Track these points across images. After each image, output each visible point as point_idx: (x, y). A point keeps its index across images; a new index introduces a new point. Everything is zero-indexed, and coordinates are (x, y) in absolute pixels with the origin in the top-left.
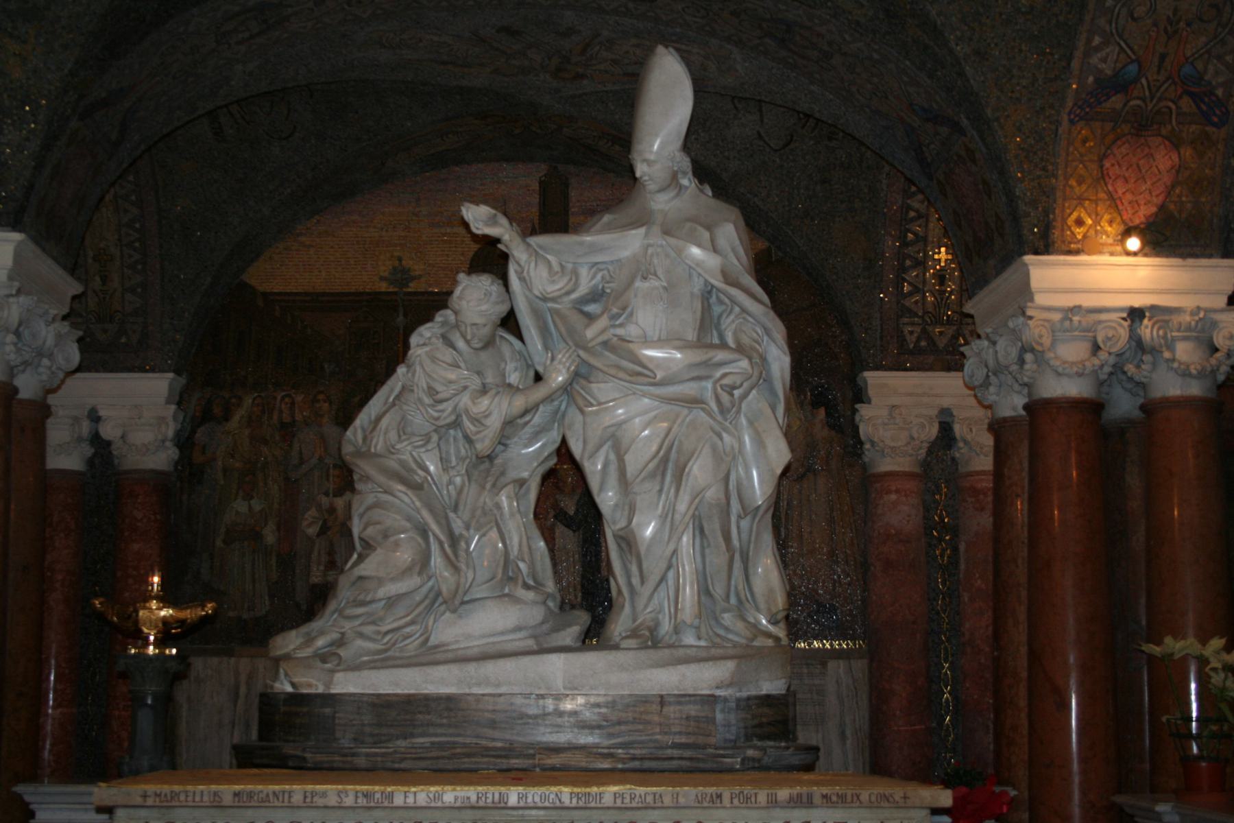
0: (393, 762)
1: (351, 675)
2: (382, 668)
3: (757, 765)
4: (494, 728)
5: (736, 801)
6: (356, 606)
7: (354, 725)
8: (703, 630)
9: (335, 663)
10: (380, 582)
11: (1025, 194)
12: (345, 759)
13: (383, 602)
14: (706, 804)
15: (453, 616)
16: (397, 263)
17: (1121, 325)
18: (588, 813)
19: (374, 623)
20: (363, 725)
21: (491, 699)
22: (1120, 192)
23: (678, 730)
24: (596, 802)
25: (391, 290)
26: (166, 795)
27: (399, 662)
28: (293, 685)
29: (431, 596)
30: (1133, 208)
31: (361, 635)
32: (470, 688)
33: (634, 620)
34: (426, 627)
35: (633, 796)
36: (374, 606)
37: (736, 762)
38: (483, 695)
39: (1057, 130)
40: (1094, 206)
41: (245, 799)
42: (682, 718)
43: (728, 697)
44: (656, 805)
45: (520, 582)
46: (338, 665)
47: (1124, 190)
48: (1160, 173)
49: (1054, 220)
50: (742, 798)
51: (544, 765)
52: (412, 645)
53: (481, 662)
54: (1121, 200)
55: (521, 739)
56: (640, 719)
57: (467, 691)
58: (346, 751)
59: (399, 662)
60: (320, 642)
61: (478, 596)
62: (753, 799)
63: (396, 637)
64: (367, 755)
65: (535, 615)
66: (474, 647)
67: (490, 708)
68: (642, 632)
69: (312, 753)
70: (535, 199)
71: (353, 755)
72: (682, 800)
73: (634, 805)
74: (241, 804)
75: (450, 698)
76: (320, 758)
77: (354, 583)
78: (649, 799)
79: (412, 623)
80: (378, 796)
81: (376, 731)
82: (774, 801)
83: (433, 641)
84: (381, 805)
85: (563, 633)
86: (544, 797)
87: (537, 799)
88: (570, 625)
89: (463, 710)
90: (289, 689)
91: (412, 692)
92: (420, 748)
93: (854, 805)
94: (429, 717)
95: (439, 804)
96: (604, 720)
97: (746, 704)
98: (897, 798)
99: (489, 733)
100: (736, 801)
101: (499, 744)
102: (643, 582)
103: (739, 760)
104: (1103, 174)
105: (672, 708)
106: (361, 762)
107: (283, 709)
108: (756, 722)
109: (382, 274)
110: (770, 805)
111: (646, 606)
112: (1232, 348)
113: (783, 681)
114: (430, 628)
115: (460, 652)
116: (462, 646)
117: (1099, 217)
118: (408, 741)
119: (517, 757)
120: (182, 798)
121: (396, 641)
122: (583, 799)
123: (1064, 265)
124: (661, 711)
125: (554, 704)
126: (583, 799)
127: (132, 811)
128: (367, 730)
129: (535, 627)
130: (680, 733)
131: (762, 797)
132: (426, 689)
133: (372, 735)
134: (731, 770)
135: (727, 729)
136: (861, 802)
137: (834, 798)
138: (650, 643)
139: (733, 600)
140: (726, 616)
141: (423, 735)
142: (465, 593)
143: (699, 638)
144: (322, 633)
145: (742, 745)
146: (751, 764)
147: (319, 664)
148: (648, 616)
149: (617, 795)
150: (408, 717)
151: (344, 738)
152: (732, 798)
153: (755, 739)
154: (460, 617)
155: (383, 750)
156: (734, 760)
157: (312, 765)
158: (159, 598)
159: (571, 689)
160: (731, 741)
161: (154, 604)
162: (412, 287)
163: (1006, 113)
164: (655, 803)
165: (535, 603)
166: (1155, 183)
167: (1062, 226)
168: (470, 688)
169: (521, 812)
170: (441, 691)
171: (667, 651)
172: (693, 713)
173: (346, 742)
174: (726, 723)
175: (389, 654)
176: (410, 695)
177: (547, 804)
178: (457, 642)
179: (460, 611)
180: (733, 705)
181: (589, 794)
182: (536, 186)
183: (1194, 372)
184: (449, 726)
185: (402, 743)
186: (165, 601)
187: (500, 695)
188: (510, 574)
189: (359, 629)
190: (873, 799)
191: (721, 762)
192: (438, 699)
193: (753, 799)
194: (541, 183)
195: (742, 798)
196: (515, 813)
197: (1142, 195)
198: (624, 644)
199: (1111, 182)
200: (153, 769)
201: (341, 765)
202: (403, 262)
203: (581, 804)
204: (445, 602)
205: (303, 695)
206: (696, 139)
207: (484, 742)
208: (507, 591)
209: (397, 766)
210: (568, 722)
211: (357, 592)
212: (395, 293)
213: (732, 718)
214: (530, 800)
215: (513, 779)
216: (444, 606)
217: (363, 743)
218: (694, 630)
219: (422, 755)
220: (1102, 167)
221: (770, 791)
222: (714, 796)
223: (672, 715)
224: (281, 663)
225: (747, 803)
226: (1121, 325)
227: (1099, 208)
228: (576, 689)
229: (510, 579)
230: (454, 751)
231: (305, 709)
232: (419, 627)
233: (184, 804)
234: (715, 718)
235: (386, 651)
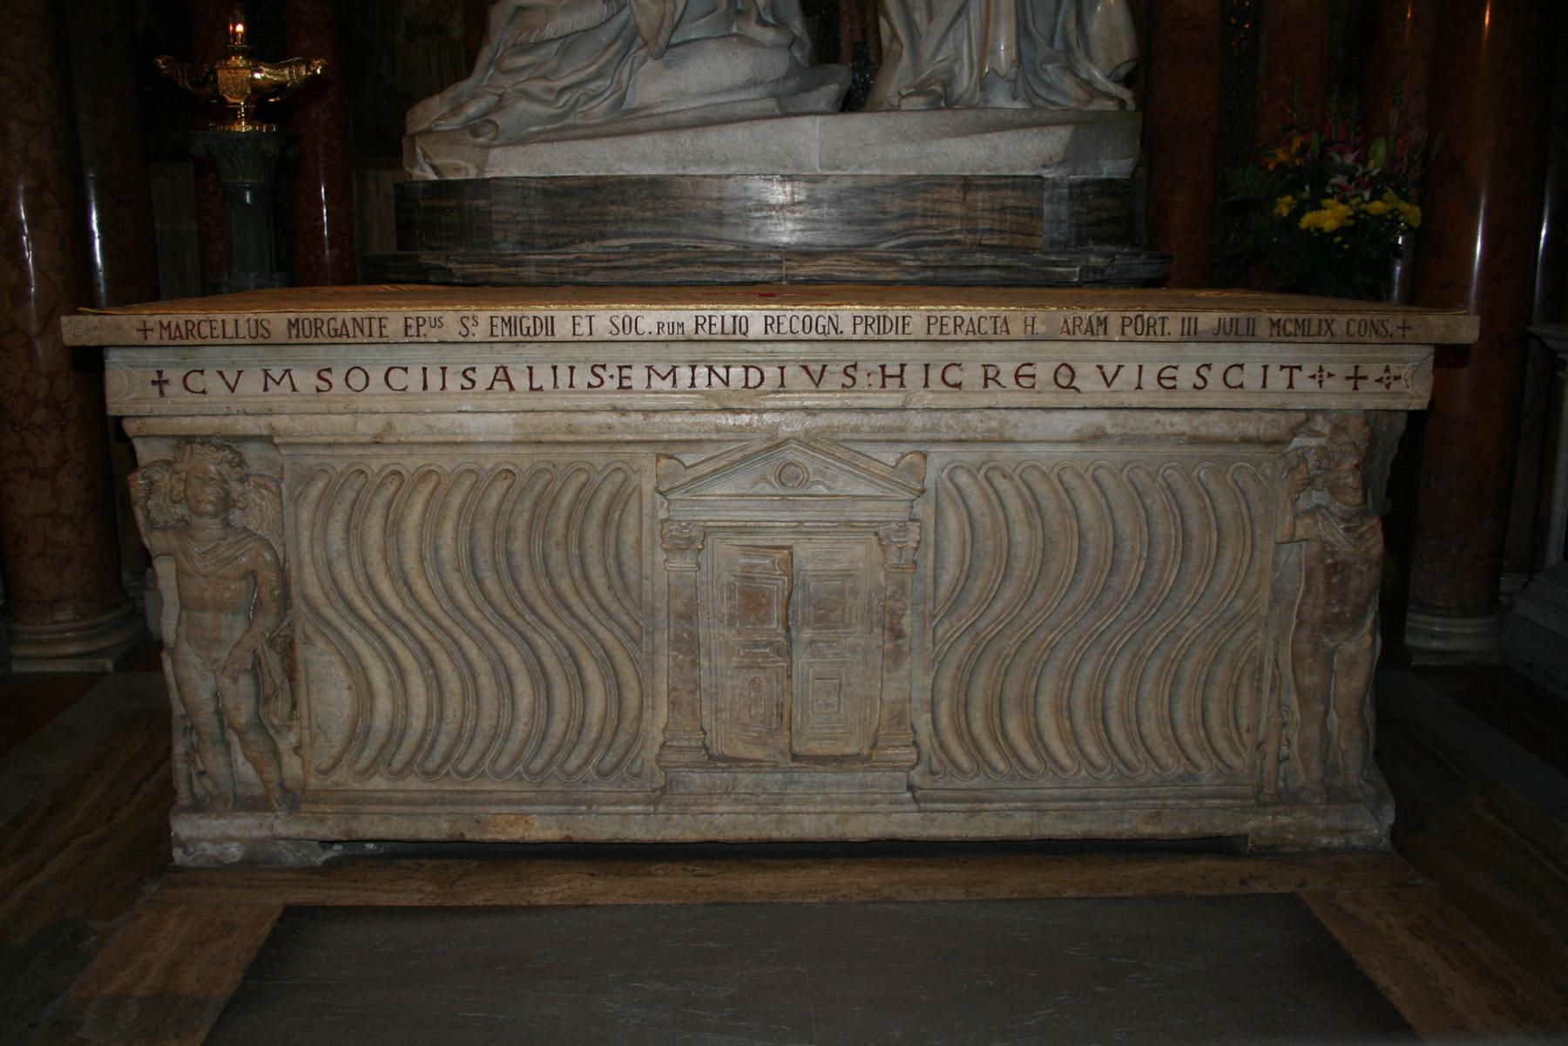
0: (576, 274)
1: (514, 152)
2: (558, 140)
3: (1099, 277)
4: (721, 225)
5: (1129, 331)
6: (517, 54)
7: (518, 222)
8: (1020, 85)
9: (491, 135)
10: (549, 12)
12: (506, 270)
13: (556, 46)
14: (1079, 336)
15: (658, 64)
18: (880, 347)
19: (544, 77)
20: (532, 222)
21: (716, 182)
23: (988, 227)
24: (897, 332)
26: (178, 327)
27: (581, 132)
28: (435, 169)
29: (626, 33)
31: (526, 95)
32: (684, 168)
33: (916, 74)
34: (619, 82)
35: (959, 321)
36: (543, 51)
38: (704, 176)
41: (307, 332)
42: (992, 210)
43: (1057, 179)
44: (998, 337)
45: (754, 17)
46: (495, 138)
50: (1139, 326)
51: (794, 276)
52: (599, 109)
53: (700, 129)
55: (760, 240)
56: (933, 211)
57: (681, 172)
58: (506, 259)
59: (581, 132)
60: (472, 110)
61: (693, 37)
62: (1158, 328)
63: (576, 96)
64: (538, 264)
65: (776, 64)
66: (690, 109)
67: (715, 195)
68: (933, 87)
69: (459, 262)
71: (519, 264)
72: (1040, 328)
73: (960, 336)
74: (302, 340)
75: (654, 181)
76: (470, 268)
77: (511, 19)
78: (987, 326)
79: (599, 75)
80: (528, 323)
81: (552, 231)
83: (631, 101)
84: (535, 339)
85: (815, 95)
86: (805, 322)
87: (797, 326)
88: (824, 83)
89: (675, 198)
90: (433, 177)
91: (602, 173)
92: (614, 253)
93: (1322, 339)
94: (627, 209)
95: (633, 336)
96: (881, 212)
97: (1079, 191)
98: (1391, 328)
99: (713, 230)
100: (1129, 331)
101: (729, 248)
102: (931, 18)
103: (1078, 269)
105: (980, 195)
106: (531, 273)
107: (422, 204)
108: (1092, 218)
110: (1185, 337)
111: (937, 50)
113: (1130, 161)
114: (625, 84)
115: (670, 118)
116: (671, 109)
118: (597, 244)
119: (756, 265)
120: (205, 330)
121: (577, 101)
122: (875, 326)
124: (964, 199)
125: (808, 189)
126: (875, 326)
127: (132, 353)
128: (538, 228)
129: (776, 82)
130: (991, 231)
131: (1174, 322)
132: (621, 170)
133: (544, 235)
134: (1063, 283)
135: (1055, 226)
136: (1333, 335)
137: (1290, 328)
138: (943, 104)
139: (1058, 45)
140: (1049, 67)
141: (617, 236)
142: (674, 29)
143: (1014, 98)
144: (474, 96)
145: (1073, 249)
146: (1091, 277)
147: (470, 139)
148: (938, 66)
149: (933, 321)
150: (596, 209)
151: (505, 241)
152: (1123, 326)
153: (1090, 241)
154: (668, 66)
155: (561, 257)
156: (1070, 269)
157: (460, 281)
158: (248, 55)
159: (830, 168)
160: (1060, 243)
161: (240, 61)
164: (995, 333)
165: (775, 46)
168: (684, 168)
169: (769, 346)
170: (643, 173)
171: (970, 113)
172: (1010, 202)
173: (507, 248)
174: (1055, 213)
175: (569, 121)
176: (597, 178)
177: (813, 335)
178: (664, 102)
179: (668, 56)
180: (1065, 191)
181: (884, 317)
184: (656, 221)
185: (588, 248)
186: (258, 52)
187: (729, 176)
188: (740, 6)
189: (522, 86)
190: (1353, 328)
191: (1053, 273)
192: (639, 182)
193: (1158, 328)
195: (1139, 326)
196: (760, 348)
198: (908, 103)
200: (259, 287)
201: (501, 279)
203: (871, 334)
204: (646, 44)
205: (447, 182)
207: (706, 245)
208: (734, 30)
209: (581, 279)
210: (828, 214)
211: (517, 32)
213: (1063, 210)
214: (785, 328)
215: (761, 295)
216: (645, 49)
217: (532, 247)
218: (1007, 85)
219: (616, 264)
221: (1186, 315)
222: (1095, 323)
223: (980, 205)
224: (417, 138)
225: (1148, 334)
228: (838, 168)
229: (739, 13)
230: (663, 257)
231: (453, 203)
232: (608, 82)
233: (209, 341)
234: (1042, 209)
235: (562, 116)
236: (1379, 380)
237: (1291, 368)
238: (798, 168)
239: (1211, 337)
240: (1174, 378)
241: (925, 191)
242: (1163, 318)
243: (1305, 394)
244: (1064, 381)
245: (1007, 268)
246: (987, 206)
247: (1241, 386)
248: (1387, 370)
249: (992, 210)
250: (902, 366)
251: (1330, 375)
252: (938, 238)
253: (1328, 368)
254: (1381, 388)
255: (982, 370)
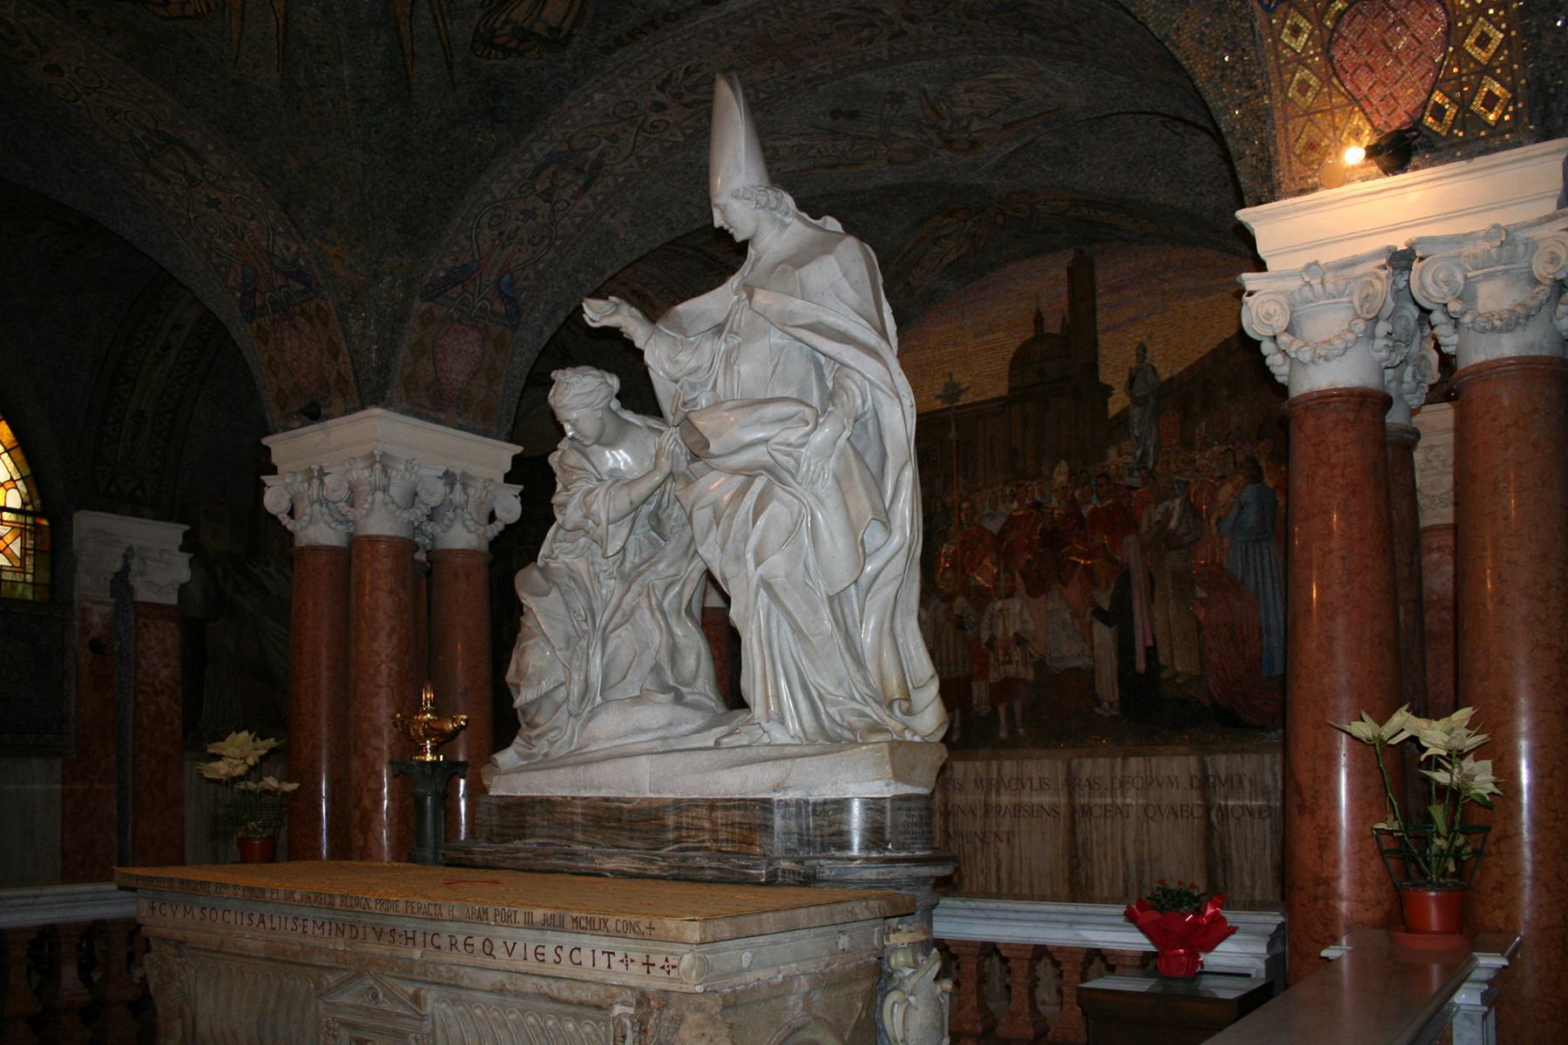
11: (1234, 128)
16: (948, 380)
17: (1378, 277)
22: (1365, 89)
25: (945, 406)
30: (1387, 105)
37: (761, 874)
39: (1252, 27)
40: (1330, 118)
47: (1370, 84)
48: (1420, 42)
49: (1276, 152)
54: (1368, 100)
70: (1064, 289)
82: (283, 920)
98: (643, 928)
104: (1334, 69)
106: (478, 859)
109: (937, 393)
112: (1562, 275)
115: (590, 755)
117: (1338, 133)
123: (1297, 210)
137: (583, 923)
162: (965, 399)
163: (1174, 26)
166: (1415, 60)
167: (1289, 158)
172: (738, 819)
182: (1064, 274)
183: (1498, 323)
185: (518, 844)
191: (748, 874)
193: (513, 918)
194: (1069, 269)
197: (1399, 84)
199: (1349, 77)
202: (954, 377)
206: (1157, 181)
212: (948, 409)
220: (1331, 60)
226: (1378, 277)
227: (1337, 120)
236: (663, 967)
237: (609, 953)
238: (636, 792)
239: (540, 926)
240: (543, 954)
241: (687, 811)
242: (515, 912)
243: (617, 973)
244: (488, 951)
245: (718, 869)
246: (724, 821)
247: (580, 963)
248: (667, 960)
249: (727, 825)
250: (414, 932)
251: (632, 961)
252: (696, 845)
253: (631, 955)
254: (663, 973)
255: (449, 939)
